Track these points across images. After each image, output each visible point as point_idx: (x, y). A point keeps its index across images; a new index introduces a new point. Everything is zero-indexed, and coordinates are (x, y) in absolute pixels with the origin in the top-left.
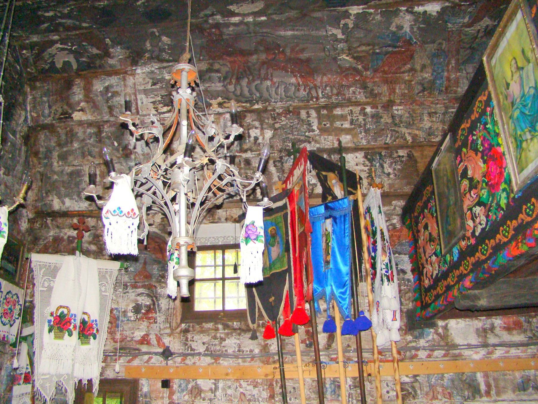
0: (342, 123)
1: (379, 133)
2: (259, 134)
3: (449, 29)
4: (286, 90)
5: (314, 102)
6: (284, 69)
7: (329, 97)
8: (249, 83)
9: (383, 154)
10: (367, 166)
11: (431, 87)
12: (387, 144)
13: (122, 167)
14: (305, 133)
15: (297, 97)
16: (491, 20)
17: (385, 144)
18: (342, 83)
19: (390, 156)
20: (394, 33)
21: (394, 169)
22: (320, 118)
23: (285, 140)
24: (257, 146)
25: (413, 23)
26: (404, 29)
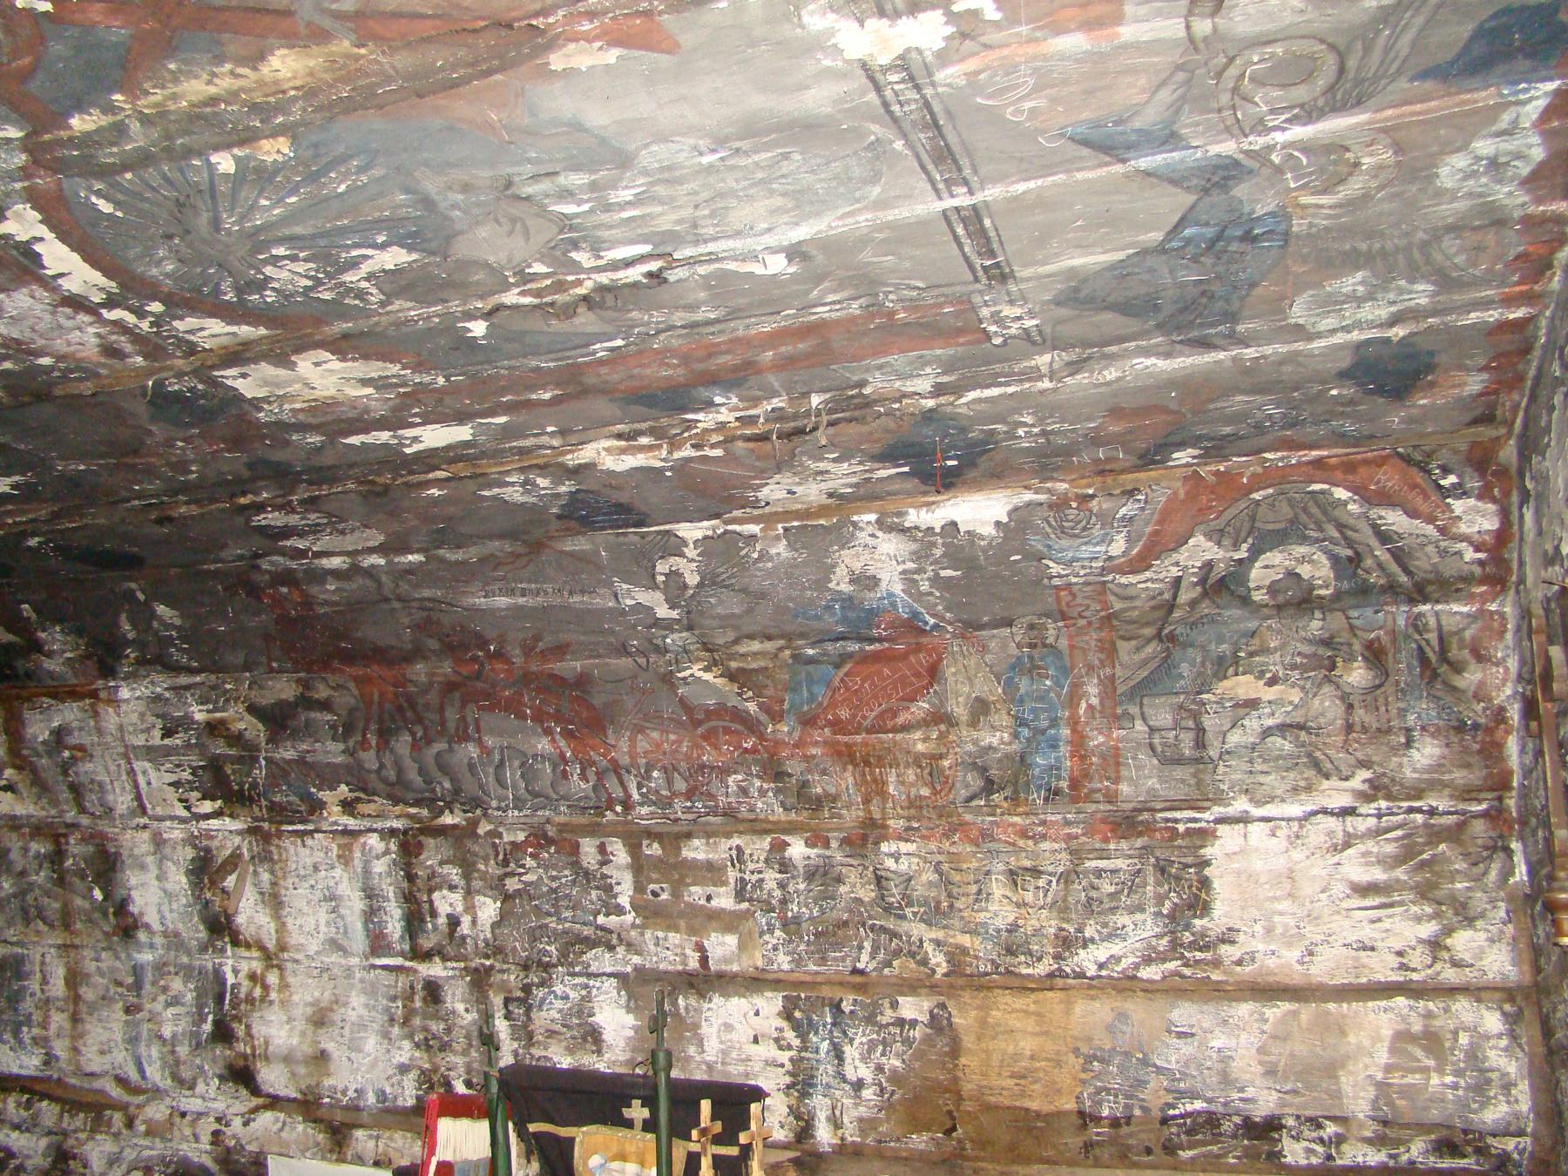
0: (710, 890)
1: (830, 936)
2: (460, 908)
3: (1056, 582)
4: (528, 774)
5: (617, 814)
6: (513, 707)
7: (666, 803)
8: (415, 746)
9: (847, 1007)
10: (789, 1047)
11: (1016, 775)
12: (862, 972)
13: (118, 964)
14: (596, 913)
15: (564, 798)
16: (1219, 544)
17: (855, 971)
18: (699, 757)
19: (870, 1020)
20: (848, 601)
21: (880, 1069)
22: (639, 866)
23: (538, 933)
24: (459, 946)
25: (911, 565)
26: (883, 585)
